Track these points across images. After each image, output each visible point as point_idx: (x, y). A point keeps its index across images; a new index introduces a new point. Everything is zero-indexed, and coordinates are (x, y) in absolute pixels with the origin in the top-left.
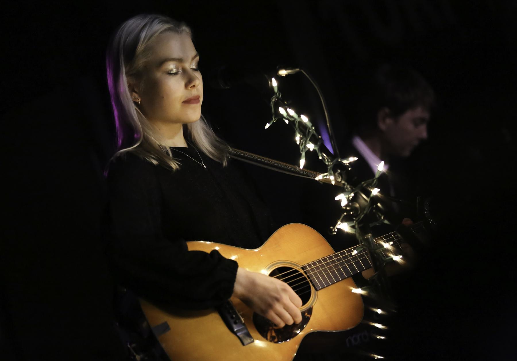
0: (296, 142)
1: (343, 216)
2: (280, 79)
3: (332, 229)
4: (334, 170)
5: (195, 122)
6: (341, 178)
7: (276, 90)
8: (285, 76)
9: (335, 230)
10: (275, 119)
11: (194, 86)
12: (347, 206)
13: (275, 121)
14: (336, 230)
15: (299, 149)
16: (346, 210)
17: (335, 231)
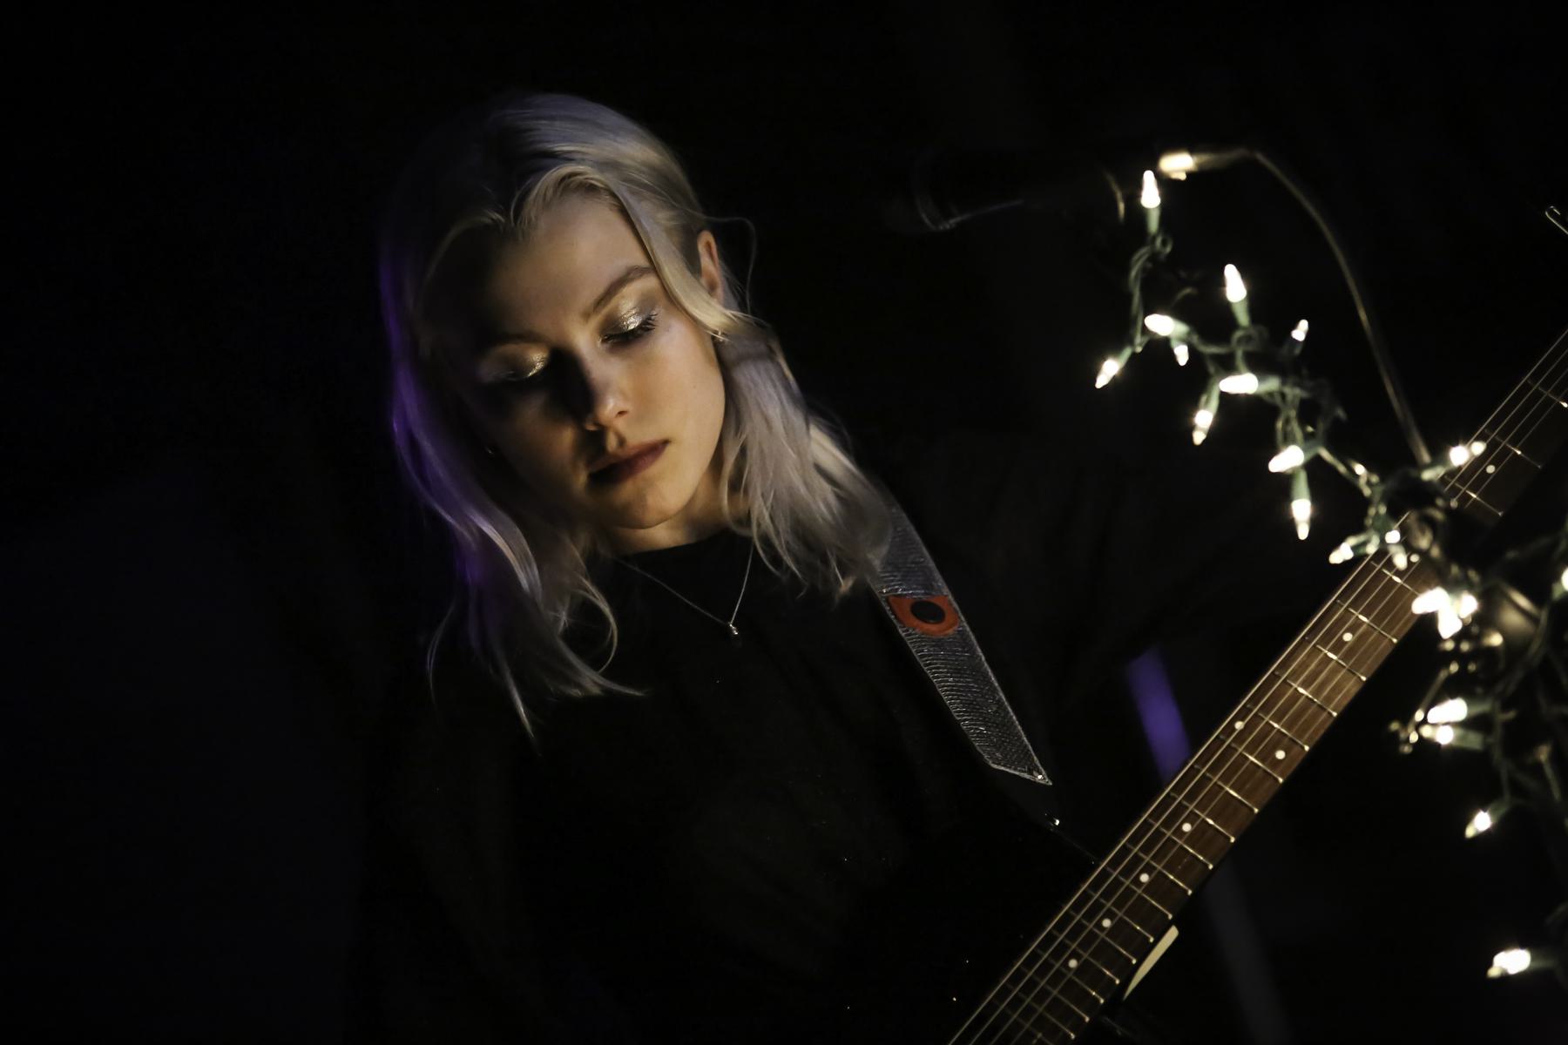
1: (1443, 675)
3: (1396, 734)
7: (1153, 223)
8: (1183, 177)
12: (1458, 638)
15: (1365, 514)
16: (1456, 655)
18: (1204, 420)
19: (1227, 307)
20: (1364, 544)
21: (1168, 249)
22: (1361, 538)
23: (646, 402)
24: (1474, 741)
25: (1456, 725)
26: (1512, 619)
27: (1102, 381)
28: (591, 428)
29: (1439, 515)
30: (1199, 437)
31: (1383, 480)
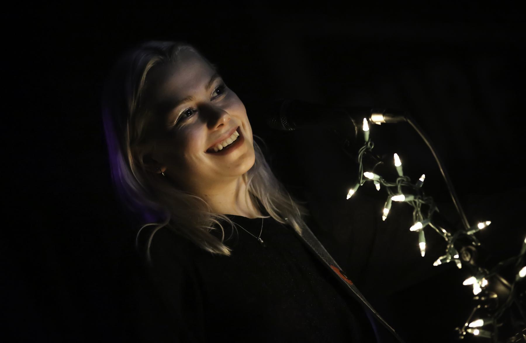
1: (475, 309)
2: (372, 125)
4: (457, 248)
6: (469, 256)
8: (380, 124)
9: (463, 333)
10: (363, 181)
11: (222, 125)
12: (480, 295)
13: (362, 185)
14: (464, 333)
16: (479, 302)
17: (462, 335)
18: (386, 211)
20: (446, 259)
21: (373, 147)
22: (445, 257)
24: (487, 335)
25: (478, 328)
26: (501, 288)
30: (384, 218)
31: (452, 235)
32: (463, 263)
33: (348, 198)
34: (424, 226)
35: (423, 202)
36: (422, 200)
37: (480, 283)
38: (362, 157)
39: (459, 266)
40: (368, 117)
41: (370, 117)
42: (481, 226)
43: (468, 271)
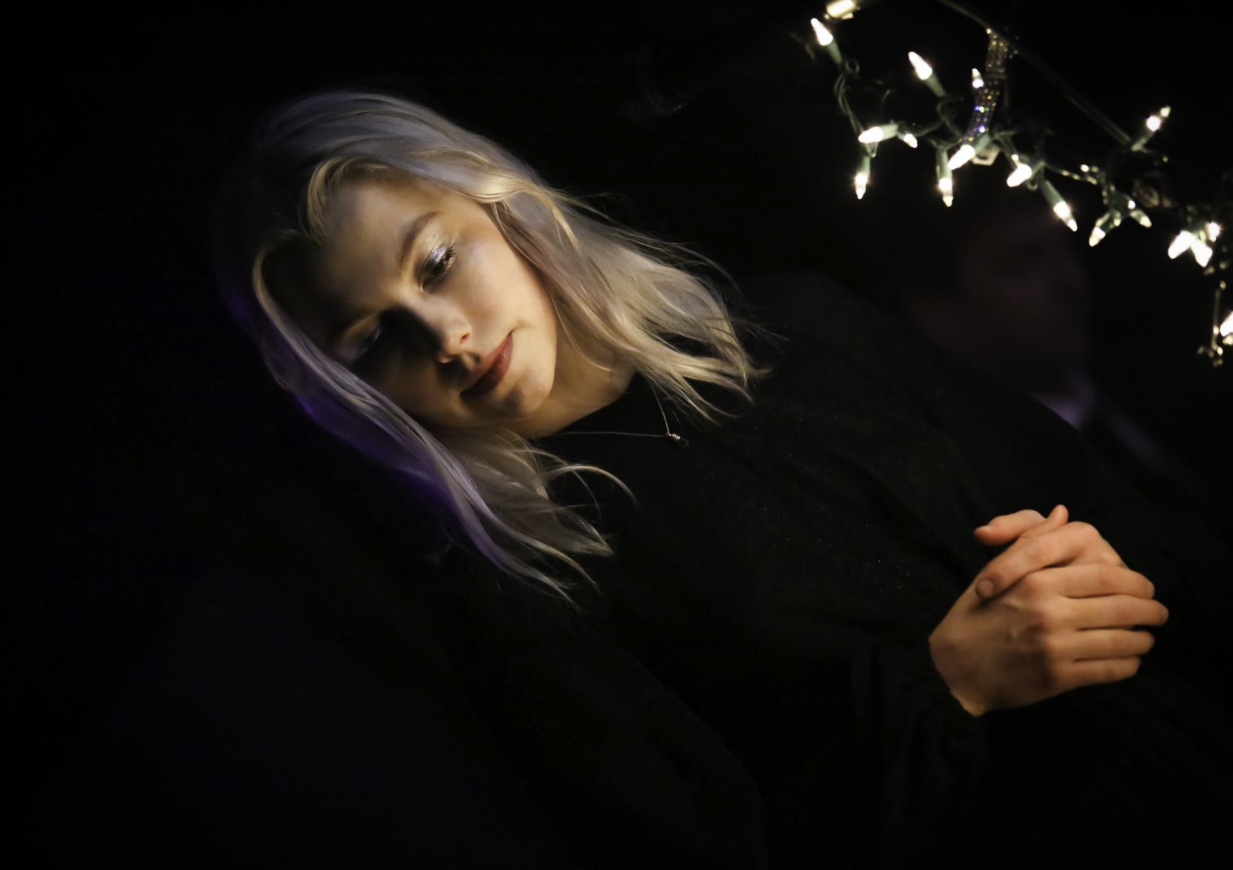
0: (939, 197)
1: (1218, 294)
3: (1205, 355)
4: (1126, 188)
5: (1068, 219)
6: (1156, 194)
7: (836, 54)
8: (850, 16)
9: (1216, 353)
12: (1213, 262)
14: (1220, 351)
16: (1219, 275)
18: (946, 186)
19: (923, 85)
20: (1111, 220)
21: (858, 68)
22: (1106, 217)
23: (481, 315)
27: (860, 193)
28: (445, 361)
29: (1156, 174)
30: (948, 201)
31: (1101, 168)
32: (1149, 213)
33: (860, 196)
34: (1036, 171)
35: (1011, 133)
36: (1006, 128)
37: (1202, 234)
38: (846, 101)
39: (1146, 222)
40: (820, 14)
41: (825, 12)
42: (1153, 124)
43: (1168, 226)
